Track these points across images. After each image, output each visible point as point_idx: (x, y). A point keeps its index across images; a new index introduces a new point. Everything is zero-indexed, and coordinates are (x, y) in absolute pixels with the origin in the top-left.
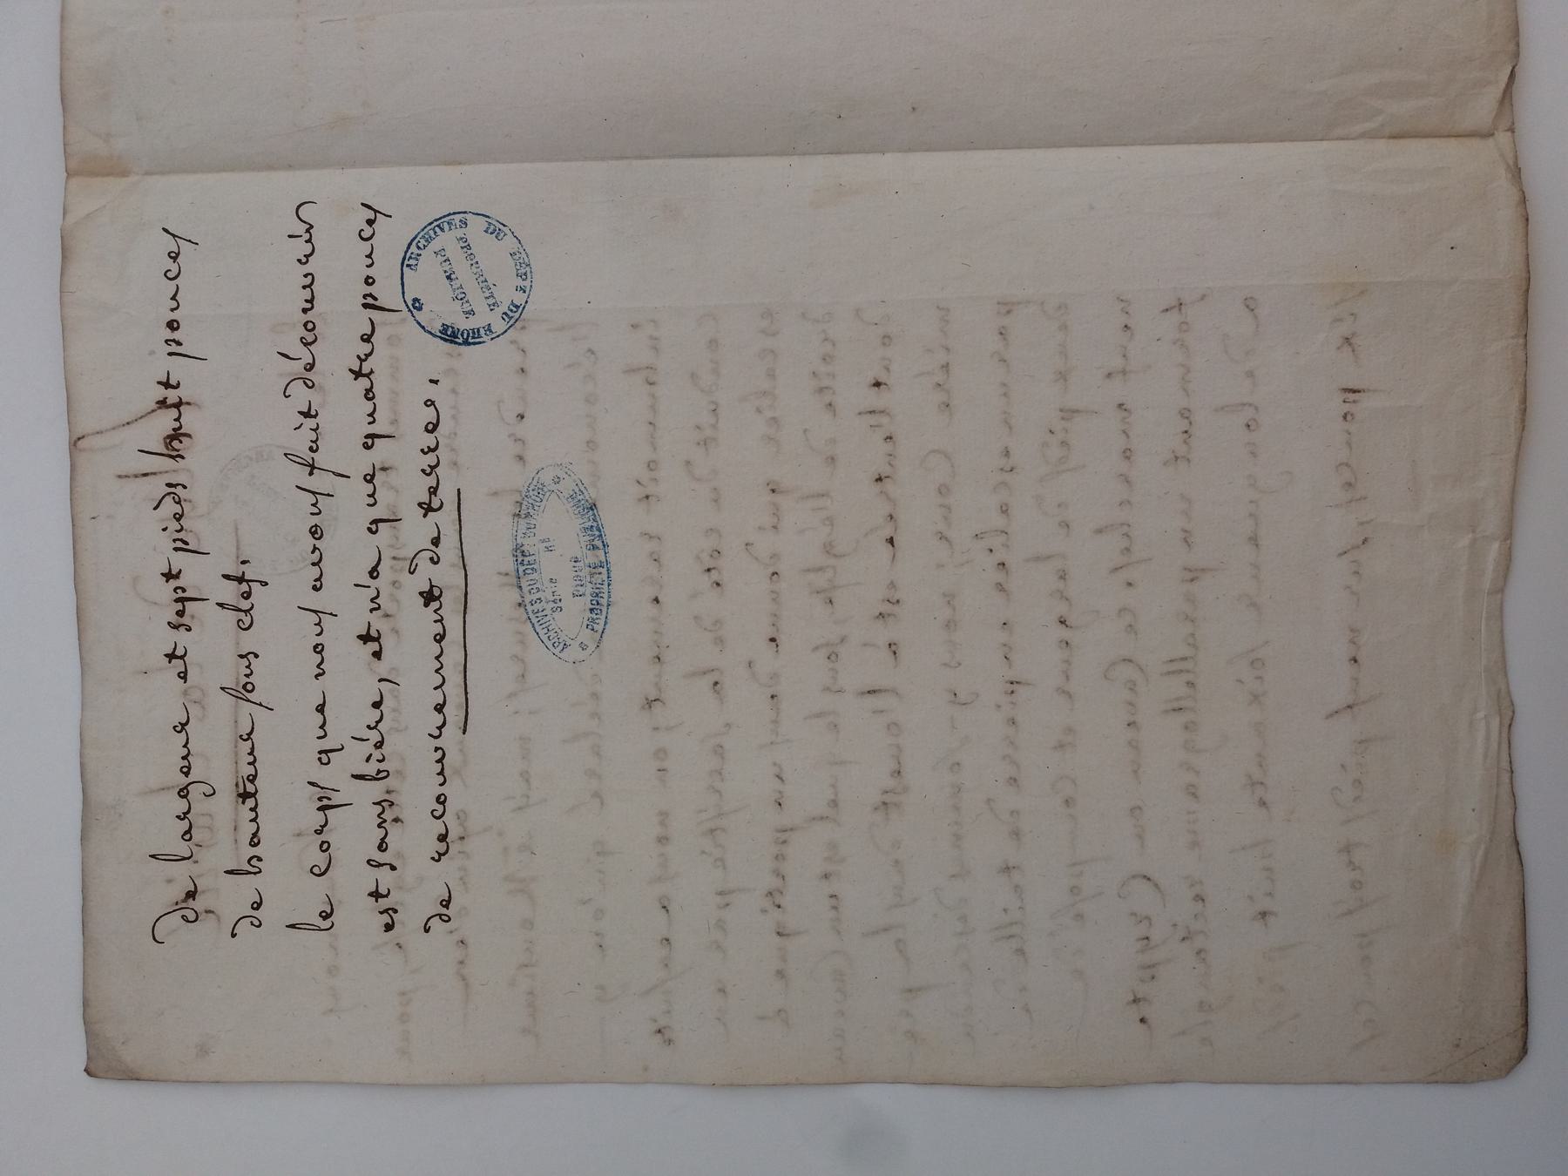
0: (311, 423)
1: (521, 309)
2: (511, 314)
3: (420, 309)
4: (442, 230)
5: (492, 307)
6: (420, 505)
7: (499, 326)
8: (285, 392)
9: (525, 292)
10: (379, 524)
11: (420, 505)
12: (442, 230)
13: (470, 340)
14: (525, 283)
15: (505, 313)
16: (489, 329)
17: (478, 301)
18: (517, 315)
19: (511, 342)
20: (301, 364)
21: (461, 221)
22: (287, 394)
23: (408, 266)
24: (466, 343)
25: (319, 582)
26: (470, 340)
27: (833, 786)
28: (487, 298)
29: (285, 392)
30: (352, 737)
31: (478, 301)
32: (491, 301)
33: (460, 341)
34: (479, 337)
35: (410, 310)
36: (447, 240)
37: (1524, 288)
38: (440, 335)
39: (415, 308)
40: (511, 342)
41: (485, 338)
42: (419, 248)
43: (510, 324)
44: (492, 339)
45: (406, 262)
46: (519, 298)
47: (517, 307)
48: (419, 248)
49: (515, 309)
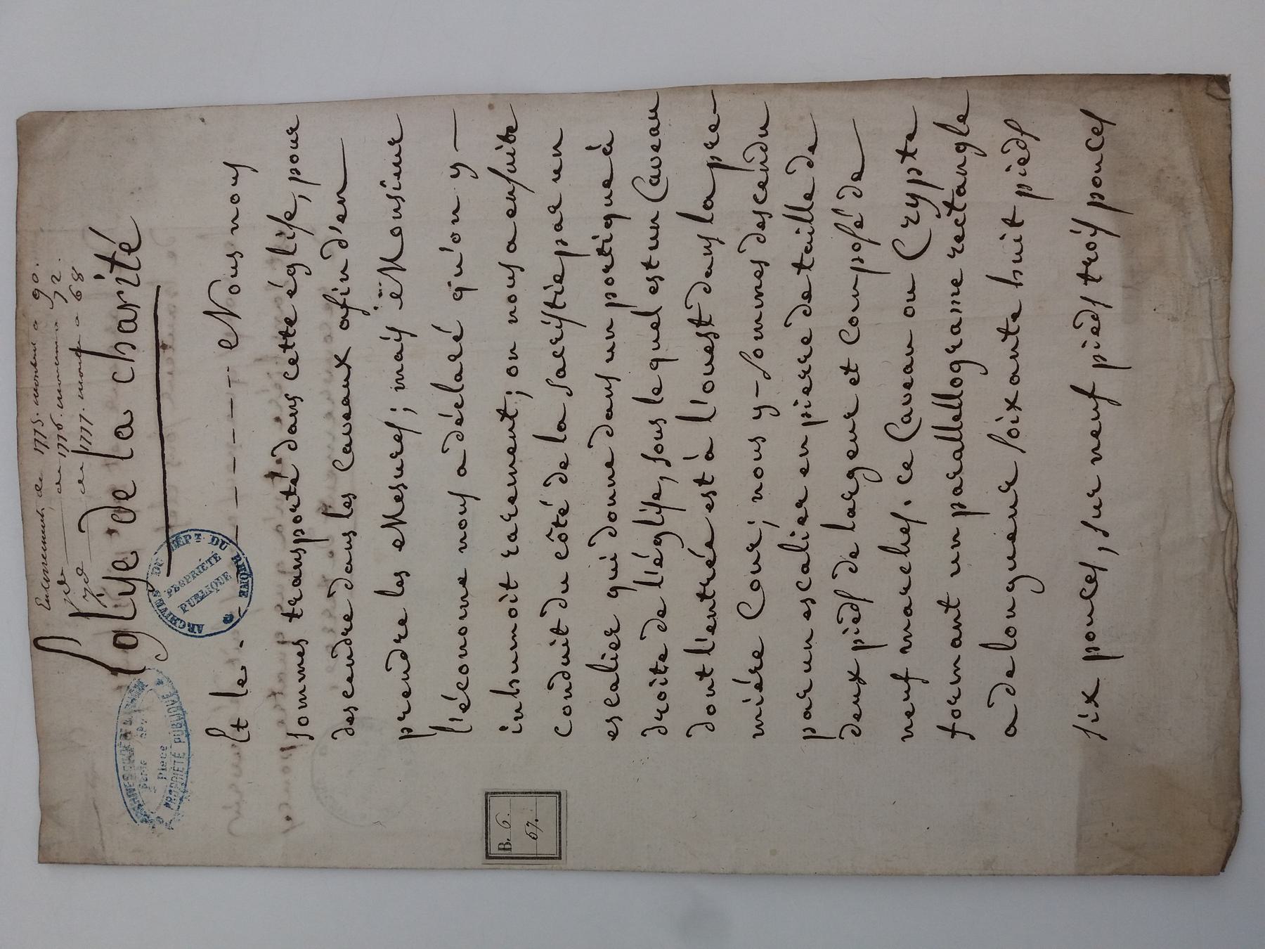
0: (1013, 233)
1: (215, 535)
2: (220, 542)
4: (166, 609)
5: (218, 559)
6: (498, 411)
8: (787, 168)
9: (200, 535)
10: (968, 147)
11: (498, 411)
14: (193, 536)
15: (220, 547)
18: (220, 537)
20: (651, 559)
22: (689, 306)
23: (200, 632)
25: (1011, 585)
29: (787, 168)
32: (213, 561)
34: (243, 565)
35: (234, 625)
36: (172, 605)
39: (231, 620)
42: (184, 626)
44: (243, 554)
45: (198, 634)
46: (207, 537)
48: (184, 626)
49: (216, 539)
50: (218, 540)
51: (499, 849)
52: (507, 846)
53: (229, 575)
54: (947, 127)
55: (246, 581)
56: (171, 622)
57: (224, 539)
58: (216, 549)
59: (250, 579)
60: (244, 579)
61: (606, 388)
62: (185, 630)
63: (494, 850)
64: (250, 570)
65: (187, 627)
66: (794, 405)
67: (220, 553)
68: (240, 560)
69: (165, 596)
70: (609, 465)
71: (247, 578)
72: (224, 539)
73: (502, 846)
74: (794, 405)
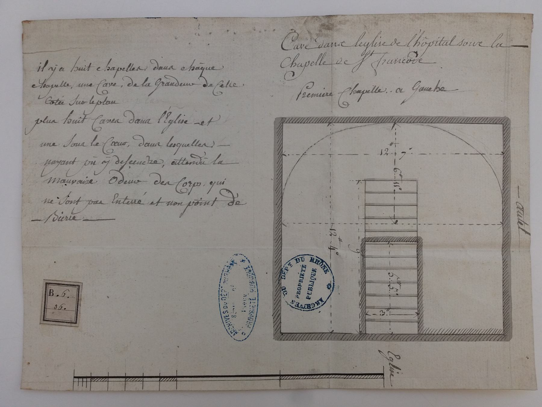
1: (295, 258)
2: (300, 259)
3: (330, 284)
7: (307, 258)
8: (166, 75)
12: (302, 305)
13: (321, 261)
16: (312, 260)
17: (308, 274)
18: (298, 257)
19: (154, 69)
21: (293, 303)
24: (323, 261)
26: (321, 261)
27: (54, 121)
28: (305, 271)
30: (358, 84)
31: (308, 274)
32: (304, 269)
33: (324, 263)
36: (303, 301)
37: (392, 180)
38: (330, 271)
39: (331, 286)
40: (154, 69)
41: (315, 258)
43: (303, 256)
46: (293, 262)
47: (296, 260)
50: (299, 259)
51: (50, 290)
52: (51, 294)
53: (314, 269)
54: (164, 114)
55: (323, 265)
56: (308, 308)
57: (301, 256)
58: (301, 263)
59: (324, 263)
60: (322, 265)
61: (139, 67)
62: (316, 306)
63: (50, 287)
64: (321, 259)
65: (316, 305)
66: (63, 212)
67: (304, 263)
68: (314, 259)
69: (297, 300)
70: (54, 121)
71: (323, 264)
72: (301, 256)
73: (52, 291)
74: (63, 212)
